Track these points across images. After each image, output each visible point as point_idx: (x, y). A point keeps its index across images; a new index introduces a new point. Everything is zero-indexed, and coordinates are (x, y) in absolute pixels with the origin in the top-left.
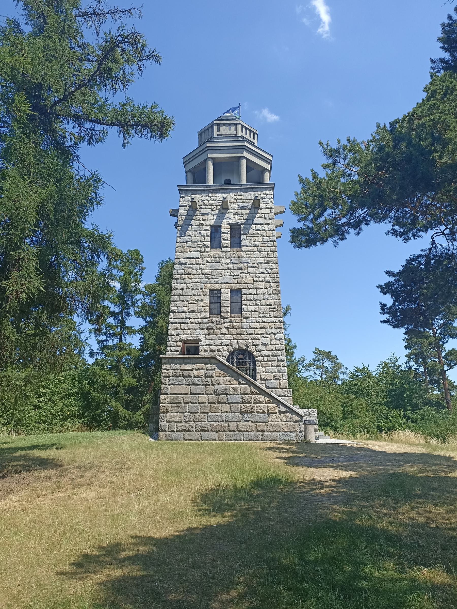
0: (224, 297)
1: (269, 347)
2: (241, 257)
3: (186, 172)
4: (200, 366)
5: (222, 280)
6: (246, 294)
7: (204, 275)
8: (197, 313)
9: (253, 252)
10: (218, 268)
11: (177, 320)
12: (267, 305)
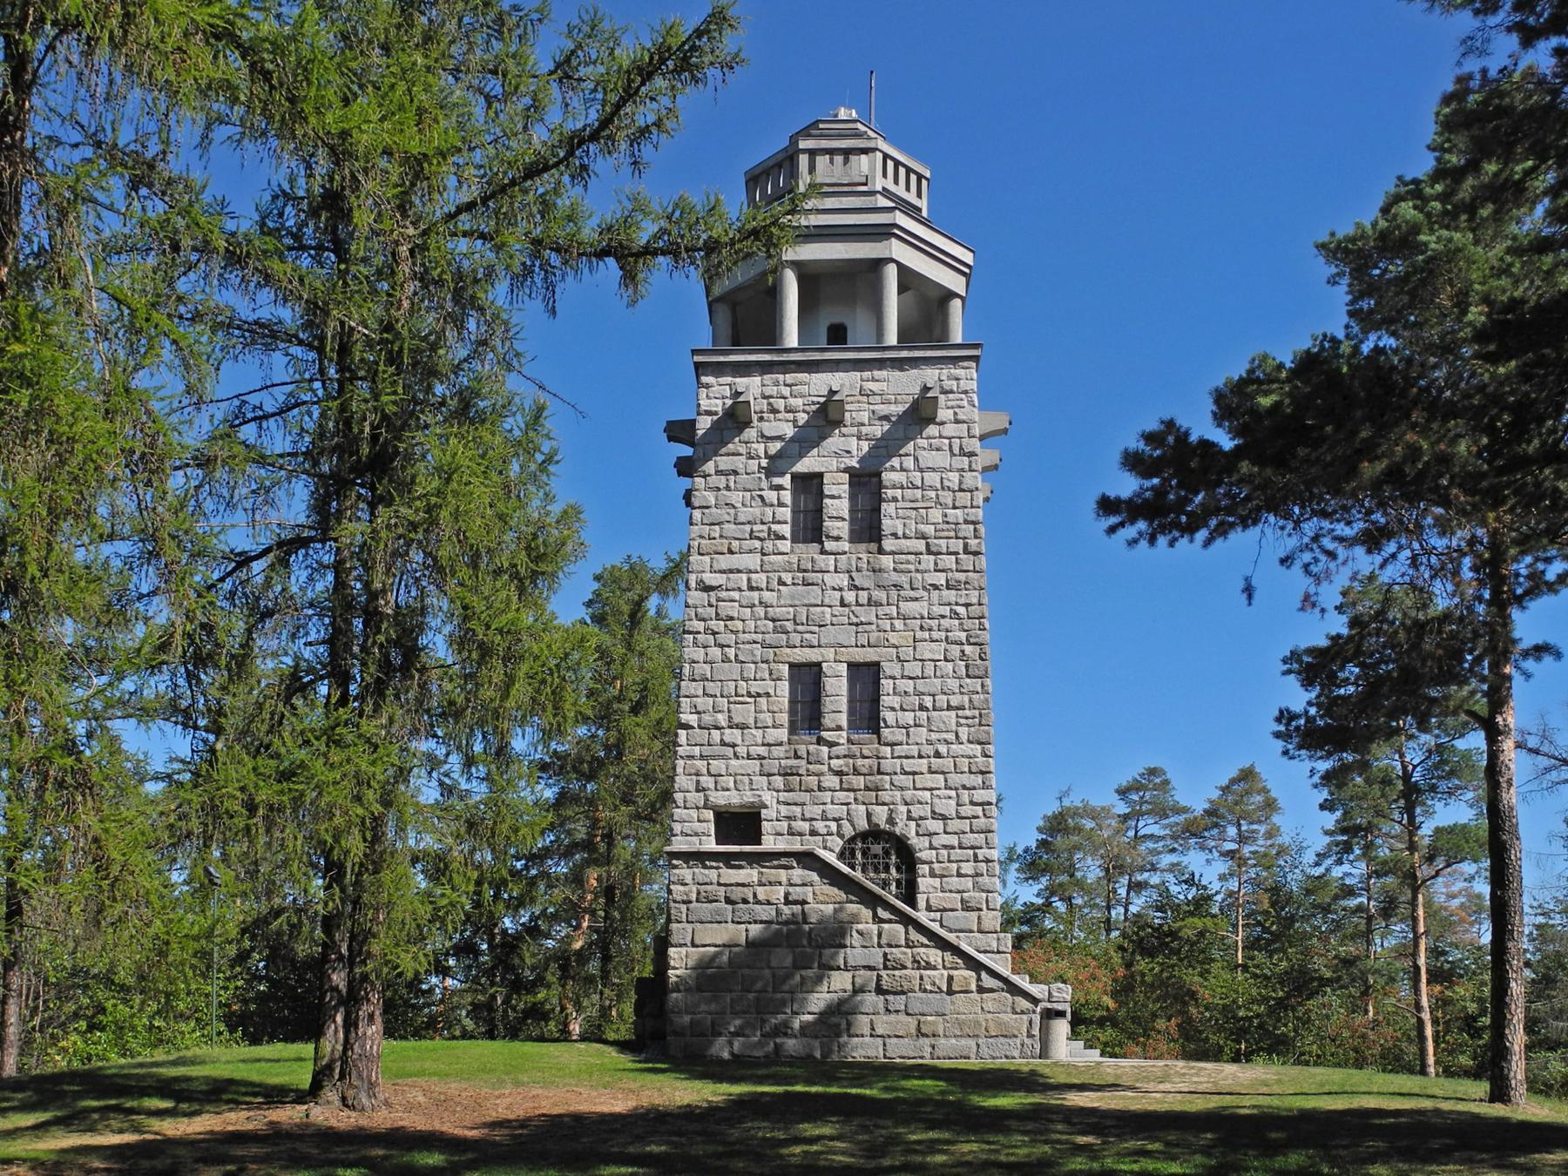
1: (954, 825)
2: (880, 570)
4: (771, 873)
5: (829, 635)
6: (894, 678)
7: (774, 620)
8: (754, 731)
10: (813, 601)
12: (949, 708)
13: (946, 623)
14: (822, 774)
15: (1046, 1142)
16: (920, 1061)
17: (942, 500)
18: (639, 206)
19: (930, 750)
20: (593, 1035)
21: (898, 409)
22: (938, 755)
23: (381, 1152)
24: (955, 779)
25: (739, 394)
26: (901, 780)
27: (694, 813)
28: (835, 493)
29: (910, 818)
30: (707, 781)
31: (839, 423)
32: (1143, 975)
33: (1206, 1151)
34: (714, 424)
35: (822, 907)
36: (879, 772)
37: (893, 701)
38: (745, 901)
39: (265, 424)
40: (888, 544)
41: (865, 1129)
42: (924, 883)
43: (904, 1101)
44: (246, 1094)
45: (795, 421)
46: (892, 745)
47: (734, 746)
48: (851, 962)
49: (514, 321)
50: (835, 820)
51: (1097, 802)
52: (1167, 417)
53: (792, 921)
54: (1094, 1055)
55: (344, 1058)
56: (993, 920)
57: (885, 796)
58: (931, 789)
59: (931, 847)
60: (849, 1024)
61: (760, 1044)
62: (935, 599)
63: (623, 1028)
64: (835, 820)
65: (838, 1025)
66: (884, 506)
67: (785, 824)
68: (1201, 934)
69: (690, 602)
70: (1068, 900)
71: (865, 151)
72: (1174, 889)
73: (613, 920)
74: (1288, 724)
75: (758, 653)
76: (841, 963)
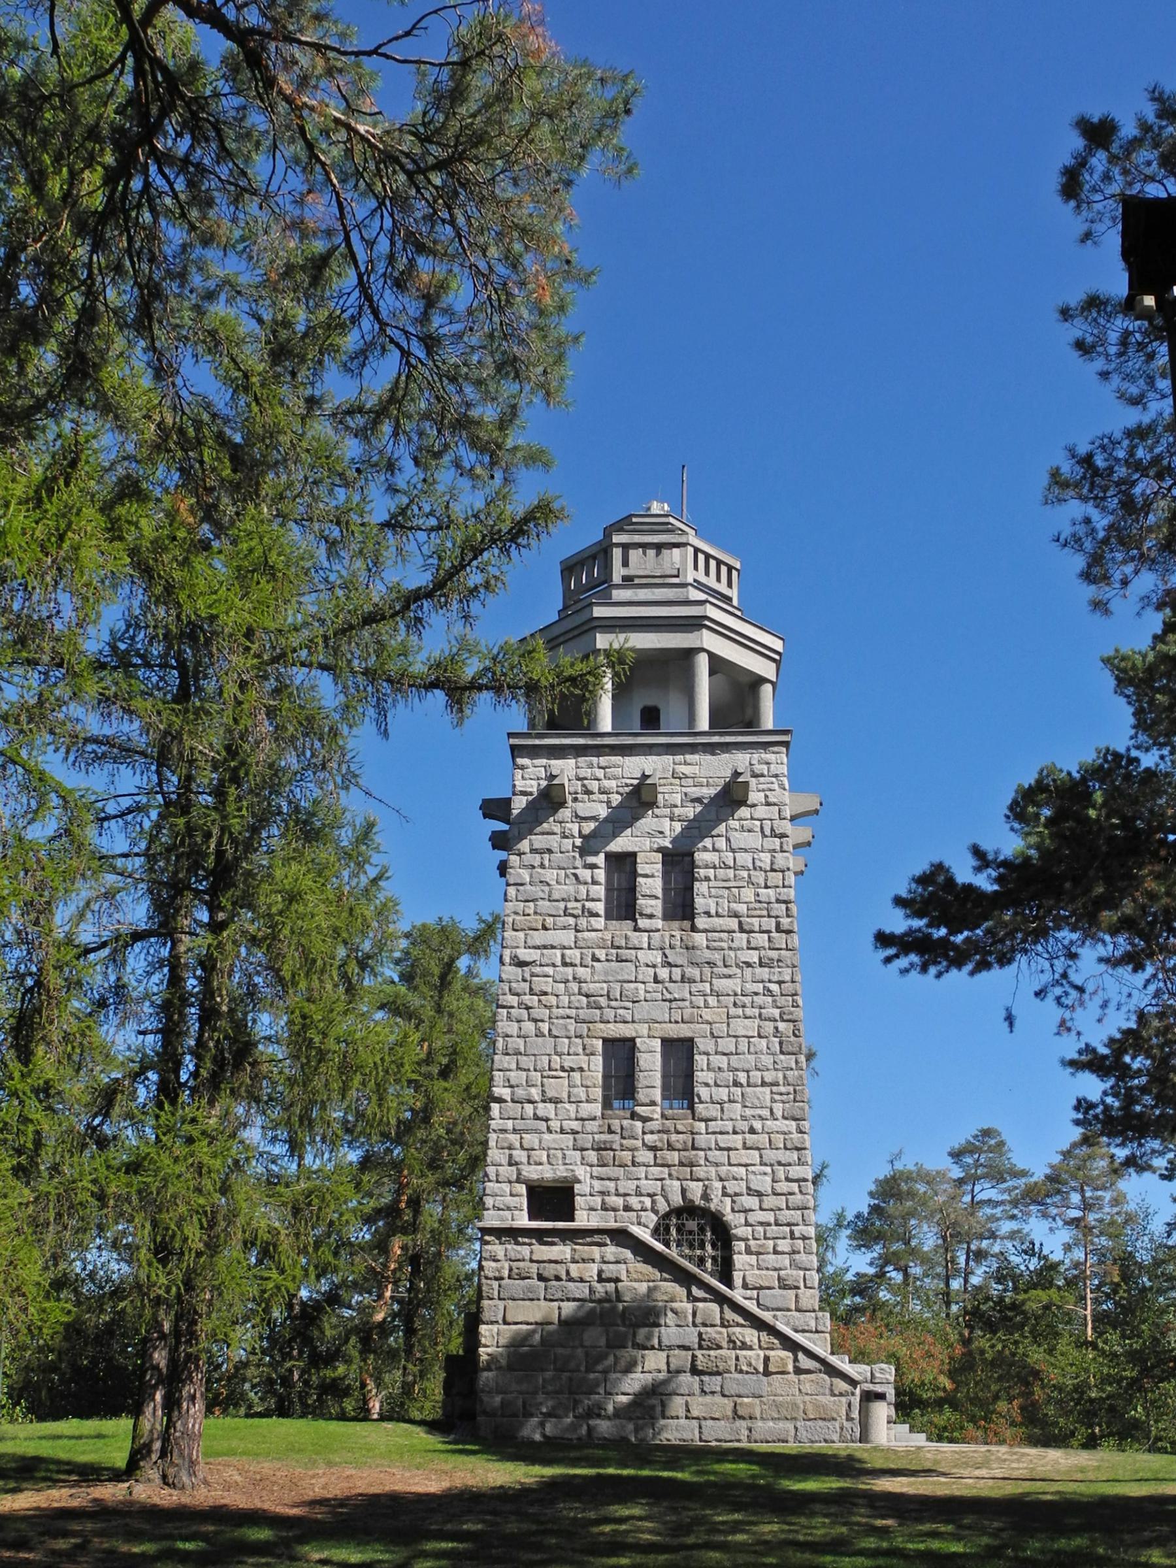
1: (770, 1202)
2: (693, 948)
5: (643, 1010)
6: (708, 1054)
8: (567, 1106)
10: (626, 977)
11: (509, 1124)
12: (764, 1084)
13: (759, 1000)
14: (636, 1149)
15: (845, 1524)
16: (736, 1445)
17: (754, 880)
18: (465, 646)
19: (743, 1126)
20: (394, 1413)
21: (710, 792)
22: (752, 1131)
23: (211, 1528)
24: (771, 1155)
25: (553, 777)
26: (715, 1155)
27: (506, 1187)
28: (648, 872)
29: (725, 1194)
31: (652, 804)
32: (982, 1352)
33: (995, 1534)
34: (529, 803)
35: (635, 1285)
36: (694, 1148)
37: (709, 1077)
38: (558, 1278)
39: (106, 824)
40: (701, 922)
41: (674, 1510)
42: (740, 1260)
43: (713, 1484)
44: (59, 1472)
45: (608, 802)
46: (706, 1120)
47: (547, 1120)
49: (349, 747)
50: (649, 1195)
52: (936, 860)
53: (607, 1299)
54: (920, 1439)
55: (166, 1437)
56: (811, 1298)
57: (700, 1172)
58: (746, 1165)
59: (747, 1224)
60: (663, 1405)
61: (574, 1427)
62: (748, 976)
63: (428, 1405)
64: (649, 1195)
65: (653, 1407)
66: (697, 885)
67: (599, 1199)
68: (1047, 1307)
69: (504, 976)
70: (905, 1271)
73: (418, 1290)
74: (1086, 1113)
75: (572, 1028)
76: (656, 1342)
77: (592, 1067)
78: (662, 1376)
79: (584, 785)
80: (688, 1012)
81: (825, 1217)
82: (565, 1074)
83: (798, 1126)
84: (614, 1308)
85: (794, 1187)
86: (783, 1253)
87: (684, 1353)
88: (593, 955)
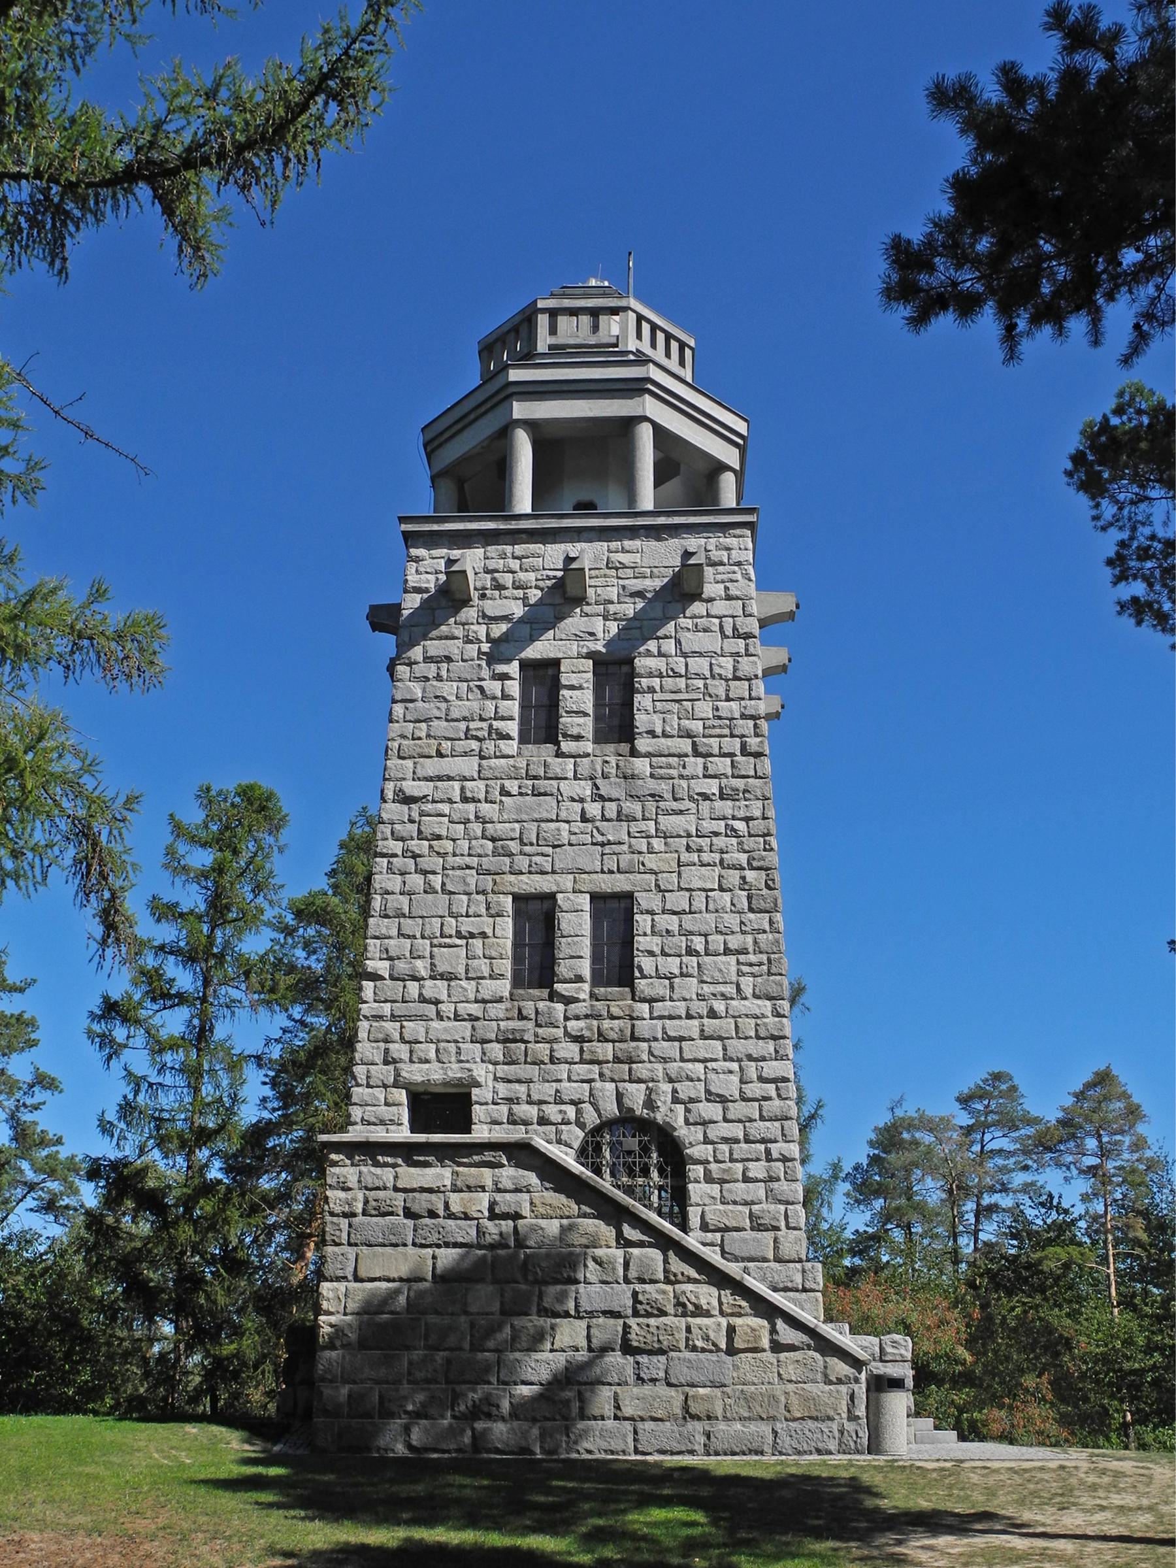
0: (566, 922)
1: (738, 1109)
2: (633, 777)
3: (433, 479)
4: (470, 1174)
5: (566, 858)
6: (651, 913)
7: (493, 840)
8: (464, 983)
9: (679, 756)
10: (545, 815)
11: (387, 1009)
12: (727, 951)
13: (720, 842)
17: (712, 690)
19: (701, 1008)
22: (712, 1014)
24: (738, 1047)
27: (380, 1094)
28: (575, 683)
29: (676, 1100)
30: (399, 1050)
31: (581, 600)
34: (424, 602)
35: (543, 1223)
36: (634, 1038)
37: (654, 943)
38: (432, 1214)
40: (643, 744)
42: (697, 1191)
45: (525, 599)
46: (651, 1001)
47: (437, 1002)
48: (585, 1306)
50: (573, 1102)
51: (934, 1111)
53: (502, 1244)
58: (705, 1061)
59: (707, 1141)
60: (581, 1398)
61: (452, 1432)
62: (705, 813)
64: (573, 1102)
65: (567, 1402)
66: (638, 697)
67: (504, 1109)
68: (1067, 1266)
71: (615, 311)
72: (1030, 1213)
75: (472, 881)
76: (571, 1306)
77: (498, 933)
78: (583, 1356)
79: (494, 579)
80: (625, 859)
81: (819, 1168)
82: (462, 942)
83: (774, 1007)
84: (515, 1256)
85: (771, 1089)
86: (757, 1180)
87: (612, 1321)
88: (502, 787)
